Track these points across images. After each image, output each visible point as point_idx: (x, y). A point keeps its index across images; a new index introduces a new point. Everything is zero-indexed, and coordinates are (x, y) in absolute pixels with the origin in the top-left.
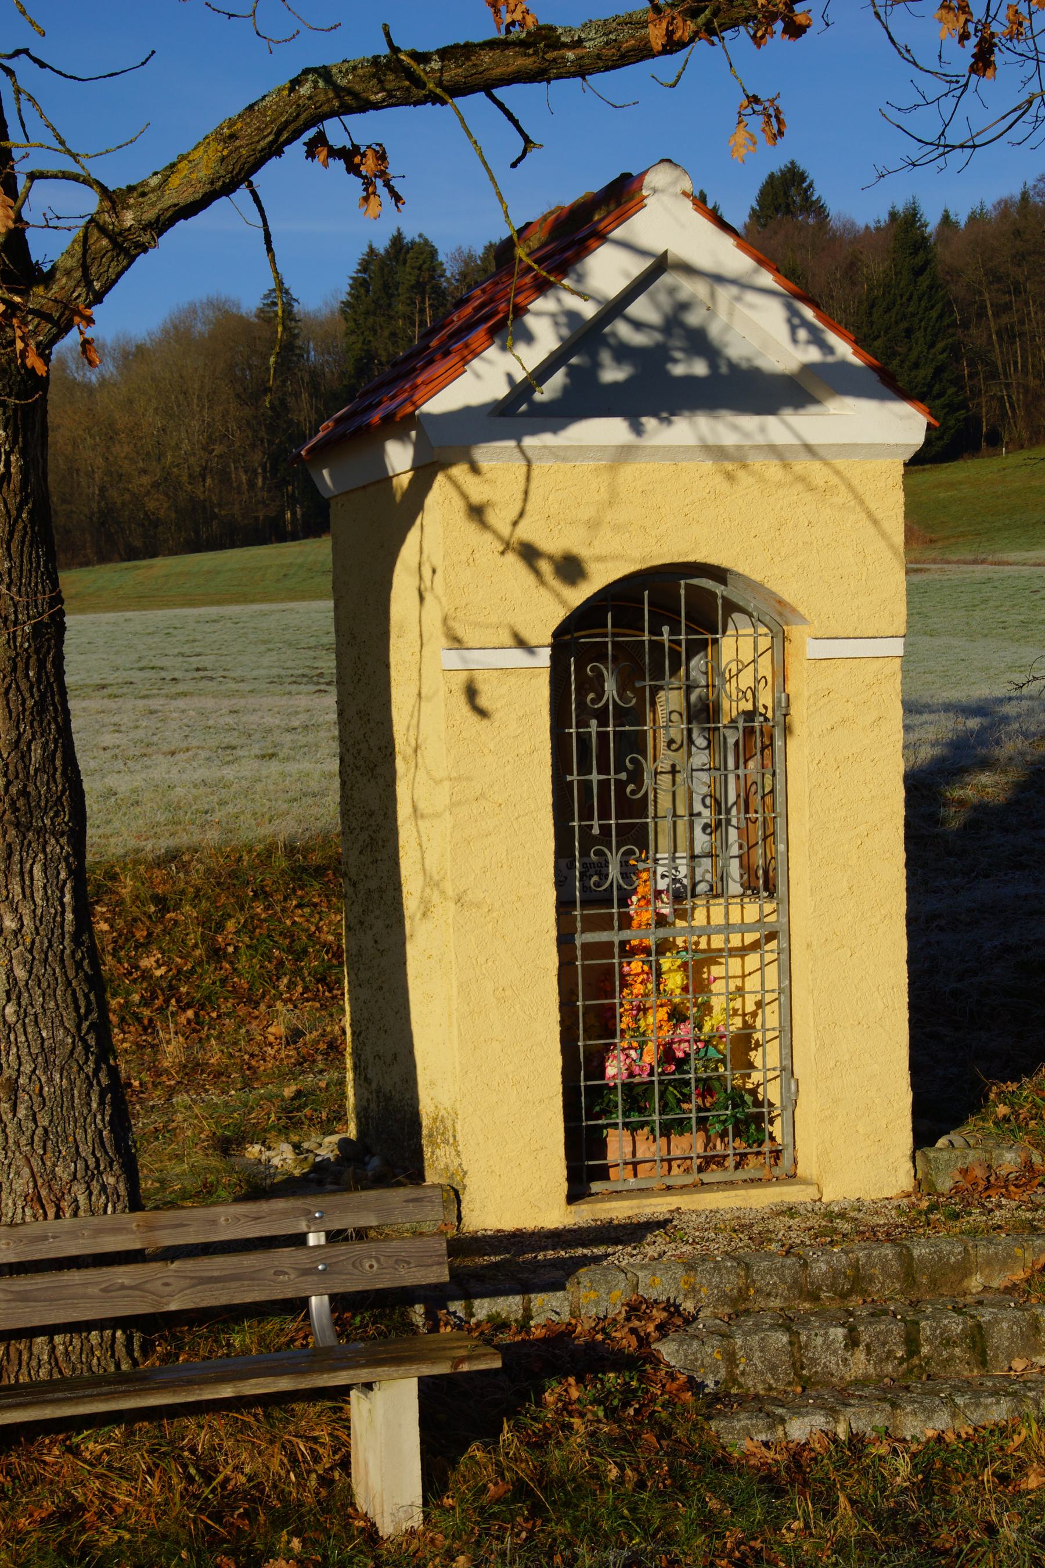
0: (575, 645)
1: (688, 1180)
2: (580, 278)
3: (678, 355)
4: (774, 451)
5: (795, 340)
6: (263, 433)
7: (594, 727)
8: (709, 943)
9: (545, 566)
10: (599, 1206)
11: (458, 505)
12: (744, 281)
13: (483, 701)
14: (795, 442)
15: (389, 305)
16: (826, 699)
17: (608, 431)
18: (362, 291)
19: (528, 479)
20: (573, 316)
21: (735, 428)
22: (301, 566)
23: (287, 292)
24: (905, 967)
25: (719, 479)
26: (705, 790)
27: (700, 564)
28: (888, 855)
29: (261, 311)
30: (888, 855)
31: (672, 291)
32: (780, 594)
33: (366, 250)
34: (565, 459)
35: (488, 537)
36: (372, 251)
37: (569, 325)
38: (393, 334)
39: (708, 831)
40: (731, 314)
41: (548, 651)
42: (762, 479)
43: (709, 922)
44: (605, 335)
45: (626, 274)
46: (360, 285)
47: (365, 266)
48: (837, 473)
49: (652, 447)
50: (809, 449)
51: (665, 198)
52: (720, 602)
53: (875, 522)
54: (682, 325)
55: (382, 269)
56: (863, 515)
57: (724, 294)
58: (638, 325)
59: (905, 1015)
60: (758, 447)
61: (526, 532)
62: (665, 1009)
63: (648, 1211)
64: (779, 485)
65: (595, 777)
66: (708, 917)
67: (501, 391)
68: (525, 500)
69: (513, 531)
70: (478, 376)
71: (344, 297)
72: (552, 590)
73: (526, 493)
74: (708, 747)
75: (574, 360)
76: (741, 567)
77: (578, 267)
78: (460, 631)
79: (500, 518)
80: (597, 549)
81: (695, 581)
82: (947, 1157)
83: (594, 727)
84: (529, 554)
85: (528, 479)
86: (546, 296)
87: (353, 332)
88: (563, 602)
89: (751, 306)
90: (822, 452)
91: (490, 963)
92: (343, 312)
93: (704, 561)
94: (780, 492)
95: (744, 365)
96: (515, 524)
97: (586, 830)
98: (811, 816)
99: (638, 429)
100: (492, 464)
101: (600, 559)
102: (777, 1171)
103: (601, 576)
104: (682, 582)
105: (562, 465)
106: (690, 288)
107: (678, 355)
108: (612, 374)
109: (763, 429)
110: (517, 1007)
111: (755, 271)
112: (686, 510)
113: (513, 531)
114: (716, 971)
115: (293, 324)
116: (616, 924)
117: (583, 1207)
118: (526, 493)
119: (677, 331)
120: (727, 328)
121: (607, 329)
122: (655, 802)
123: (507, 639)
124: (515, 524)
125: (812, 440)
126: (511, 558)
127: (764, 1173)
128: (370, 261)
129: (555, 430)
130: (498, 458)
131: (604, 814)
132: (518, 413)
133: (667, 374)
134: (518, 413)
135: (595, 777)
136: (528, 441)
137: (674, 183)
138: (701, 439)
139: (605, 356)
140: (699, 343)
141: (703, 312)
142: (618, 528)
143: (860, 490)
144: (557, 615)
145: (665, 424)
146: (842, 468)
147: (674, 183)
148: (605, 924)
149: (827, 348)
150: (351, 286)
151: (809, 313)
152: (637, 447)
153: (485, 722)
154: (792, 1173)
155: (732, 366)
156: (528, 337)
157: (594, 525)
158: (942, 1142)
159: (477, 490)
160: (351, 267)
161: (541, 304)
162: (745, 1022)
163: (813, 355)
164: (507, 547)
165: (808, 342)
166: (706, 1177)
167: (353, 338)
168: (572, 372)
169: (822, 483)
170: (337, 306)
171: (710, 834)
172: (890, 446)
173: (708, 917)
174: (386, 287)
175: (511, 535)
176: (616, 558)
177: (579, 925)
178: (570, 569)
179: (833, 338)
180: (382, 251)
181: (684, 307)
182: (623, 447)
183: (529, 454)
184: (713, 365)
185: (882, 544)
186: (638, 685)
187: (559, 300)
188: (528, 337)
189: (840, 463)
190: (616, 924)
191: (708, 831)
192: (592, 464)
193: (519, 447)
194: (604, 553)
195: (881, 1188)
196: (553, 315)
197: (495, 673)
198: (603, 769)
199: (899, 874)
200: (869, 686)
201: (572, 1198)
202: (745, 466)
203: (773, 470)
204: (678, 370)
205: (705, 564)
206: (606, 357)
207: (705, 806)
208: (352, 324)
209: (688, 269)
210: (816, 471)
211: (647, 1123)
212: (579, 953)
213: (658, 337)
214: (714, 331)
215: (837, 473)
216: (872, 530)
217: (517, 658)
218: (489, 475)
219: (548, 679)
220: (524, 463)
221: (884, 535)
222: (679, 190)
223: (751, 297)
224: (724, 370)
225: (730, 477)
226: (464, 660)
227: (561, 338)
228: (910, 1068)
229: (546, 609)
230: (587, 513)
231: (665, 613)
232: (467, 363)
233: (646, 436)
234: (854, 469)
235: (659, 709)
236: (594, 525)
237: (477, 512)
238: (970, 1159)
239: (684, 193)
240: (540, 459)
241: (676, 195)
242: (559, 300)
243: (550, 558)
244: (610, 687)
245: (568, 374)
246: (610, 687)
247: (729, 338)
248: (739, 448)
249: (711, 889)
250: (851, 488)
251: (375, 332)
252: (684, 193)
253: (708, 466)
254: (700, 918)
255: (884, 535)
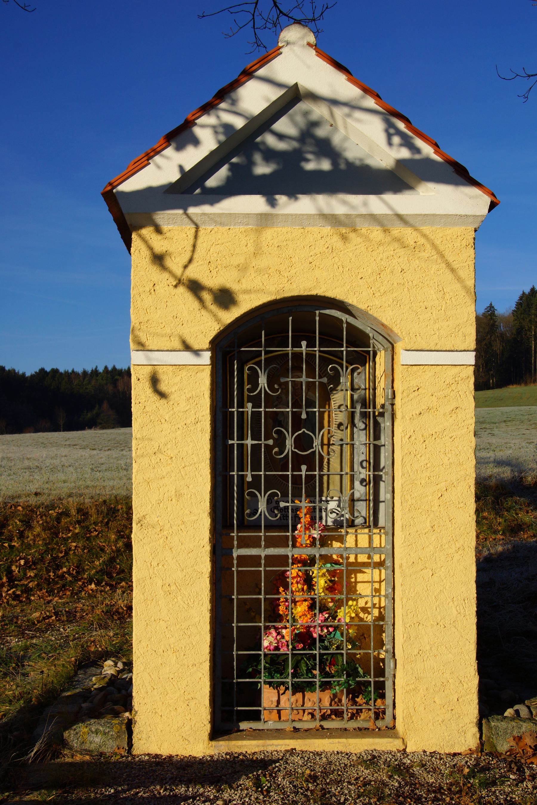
0: (231, 350)
1: (312, 725)
2: (234, 102)
3: (310, 156)
4: (374, 218)
5: (390, 144)
6: (483, 354)
7: (249, 407)
8: (356, 558)
9: (207, 297)
10: (233, 743)
11: (146, 253)
12: (353, 103)
13: (163, 387)
14: (388, 212)
15: (529, 311)
16: (416, 393)
17: (254, 203)
18: (520, 306)
19: (196, 237)
20: (228, 128)
21: (345, 203)
22: (492, 398)
23: (493, 307)
24: (474, 586)
25: (336, 238)
26: (363, 457)
27: (320, 296)
28: (462, 505)
29: (484, 314)
30: (462, 505)
31: (306, 114)
32: (380, 319)
33: (522, 293)
34: (222, 224)
35: (166, 275)
36: (524, 293)
37: (225, 133)
38: (530, 321)
39: (364, 484)
40: (346, 127)
41: (208, 354)
42: (367, 239)
43: (356, 544)
44: (257, 144)
45: (267, 100)
46: (519, 305)
47: (521, 298)
48: (424, 236)
49: (282, 215)
50: (400, 217)
51: (296, 48)
52: (345, 326)
53: (453, 270)
54: (313, 136)
55: (527, 299)
56: (444, 265)
57: (339, 112)
58: (281, 137)
59: (474, 620)
60: (362, 216)
61: (194, 272)
62: (306, 603)
63: (270, 749)
64: (380, 244)
65: (249, 442)
66: (356, 541)
67: (174, 176)
68: (193, 251)
69: (184, 271)
70: (159, 167)
71: (514, 309)
72: (211, 312)
73: (194, 246)
74: (365, 429)
75: (234, 160)
76: (351, 300)
77: (233, 95)
78: (143, 339)
79: (175, 264)
80: (246, 284)
81: (327, 312)
82: (505, 726)
83: (249, 407)
84: (195, 287)
85: (196, 237)
86: (209, 114)
87: (516, 320)
88: (218, 320)
89: (358, 121)
90: (411, 220)
91: (160, 566)
92: (513, 313)
93: (323, 294)
94: (381, 248)
95: (358, 163)
96: (186, 267)
97: (242, 478)
98: (403, 475)
99: (272, 203)
100: (170, 227)
101: (247, 292)
102: (380, 723)
103: (246, 303)
104: (317, 312)
105: (220, 228)
106: (319, 111)
107: (310, 156)
108: (262, 169)
109: (365, 204)
110: (179, 598)
111: (362, 97)
112: (311, 259)
113: (184, 271)
114: (360, 577)
115: (495, 318)
116: (263, 543)
117: (222, 743)
118: (194, 246)
119: (309, 140)
120: (346, 138)
121: (259, 139)
122: (328, 463)
123: (177, 344)
124: (186, 267)
125: (401, 212)
126: (181, 289)
127: (370, 725)
128: (523, 296)
129: (212, 203)
130: (170, 219)
131: (256, 467)
132: (189, 189)
133: (302, 169)
134: (189, 189)
135: (249, 442)
136: (192, 210)
137: (302, 38)
138: (319, 210)
139: (258, 158)
140: (325, 148)
141: (328, 128)
142: (259, 271)
143: (441, 248)
144: (212, 329)
145: (293, 200)
146: (428, 233)
147: (302, 38)
148: (283, 542)
149: (418, 151)
150: (516, 305)
151: (401, 125)
152: (271, 215)
153: (163, 401)
154: (391, 725)
155: (350, 165)
156: (196, 142)
157: (243, 269)
158: (509, 712)
159: (159, 244)
160: (516, 298)
161: (204, 119)
162: (380, 613)
163: (405, 153)
164: (179, 282)
165: (401, 145)
166: (327, 724)
167: (516, 322)
168: (233, 168)
169: (412, 243)
170: (511, 311)
171: (366, 486)
172: (461, 216)
173: (356, 541)
174: (528, 305)
175: (182, 275)
176: (258, 291)
177: (235, 543)
178: (225, 298)
179: (419, 143)
180: (527, 293)
181: (315, 124)
182: (261, 214)
183: (195, 219)
184: (335, 163)
185: (458, 286)
186: (283, 380)
187: (218, 117)
188: (196, 142)
189: (426, 229)
190: (263, 543)
191: (364, 484)
192: (242, 228)
193: (185, 213)
194: (249, 288)
195: (453, 746)
196: (214, 127)
197: (171, 368)
198: (256, 436)
199: (470, 519)
200: (449, 385)
201: (216, 734)
202: (355, 230)
203: (377, 234)
204: (310, 166)
205: (324, 297)
206: (258, 158)
207: (363, 468)
208: (516, 317)
209: (313, 97)
210: (409, 235)
211: (283, 683)
212: (235, 562)
213: (295, 144)
214: (336, 140)
215: (424, 236)
216: (449, 276)
217: (187, 357)
218: (168, 234)
219: (209, 373)
220: (193, 226)
221: (459, 279)
222: (305, 43)
223: (358, 114)
224: (343, 166)
225: (344, 238)
226: (149, 359)
227: (219, 142)
228: (478, 658)
229: (206, 325)
230: (240, 260)
231: (304, 332)
232: (151, 158)
233: (278, 208)
234: (437, 233)
235: (333, 403)
236: (243, 269)
237: (159, 259)
238: (523, 729)
239: (309, 44)
240: (204, 223)
241: (303, 46)
242: (218, 117)
243: (210, 290)
244: (263, 381)
245: (230, 170)
246: (263, 381)
247: (347, 145)
248: (347, 216)
249: (365, 522)
250: (434, 246)
251: (524, 320)
252: (309, 44)
253: (327, 230)
254: (350, 541)
255: (459, 279)
